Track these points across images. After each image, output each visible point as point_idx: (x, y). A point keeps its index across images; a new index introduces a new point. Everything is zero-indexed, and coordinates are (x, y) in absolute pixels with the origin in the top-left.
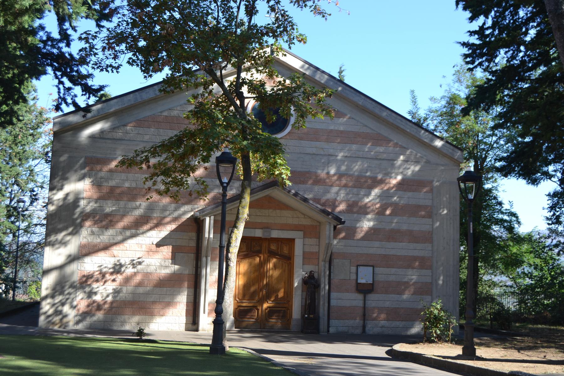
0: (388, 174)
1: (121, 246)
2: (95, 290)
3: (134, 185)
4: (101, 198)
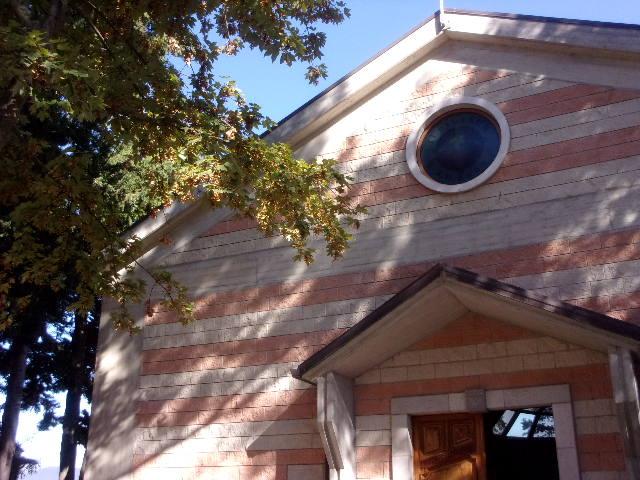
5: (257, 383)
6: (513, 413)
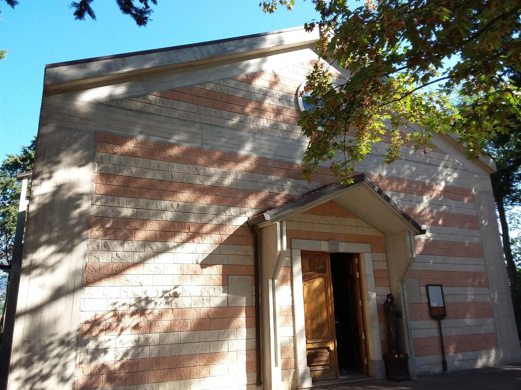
0: (435, 180)
1: (140, 269)
2: (105, 346)
3: (159, 177)
4: (112, 195)
5: (223, 217)
6: (90, 325)
